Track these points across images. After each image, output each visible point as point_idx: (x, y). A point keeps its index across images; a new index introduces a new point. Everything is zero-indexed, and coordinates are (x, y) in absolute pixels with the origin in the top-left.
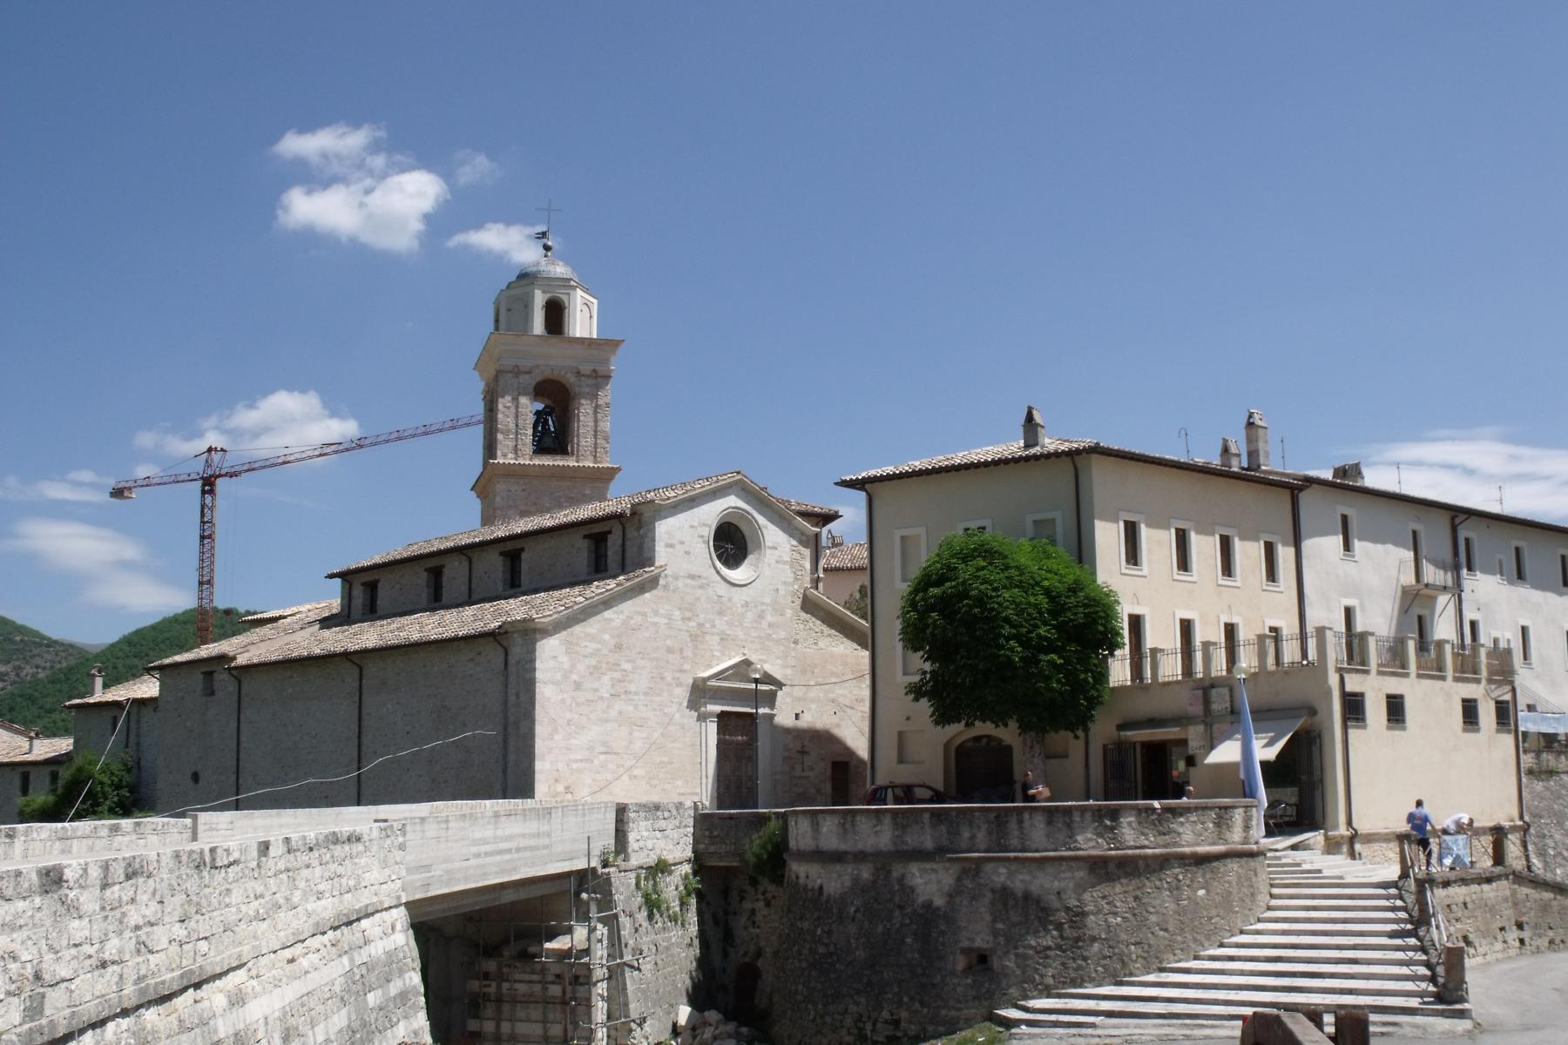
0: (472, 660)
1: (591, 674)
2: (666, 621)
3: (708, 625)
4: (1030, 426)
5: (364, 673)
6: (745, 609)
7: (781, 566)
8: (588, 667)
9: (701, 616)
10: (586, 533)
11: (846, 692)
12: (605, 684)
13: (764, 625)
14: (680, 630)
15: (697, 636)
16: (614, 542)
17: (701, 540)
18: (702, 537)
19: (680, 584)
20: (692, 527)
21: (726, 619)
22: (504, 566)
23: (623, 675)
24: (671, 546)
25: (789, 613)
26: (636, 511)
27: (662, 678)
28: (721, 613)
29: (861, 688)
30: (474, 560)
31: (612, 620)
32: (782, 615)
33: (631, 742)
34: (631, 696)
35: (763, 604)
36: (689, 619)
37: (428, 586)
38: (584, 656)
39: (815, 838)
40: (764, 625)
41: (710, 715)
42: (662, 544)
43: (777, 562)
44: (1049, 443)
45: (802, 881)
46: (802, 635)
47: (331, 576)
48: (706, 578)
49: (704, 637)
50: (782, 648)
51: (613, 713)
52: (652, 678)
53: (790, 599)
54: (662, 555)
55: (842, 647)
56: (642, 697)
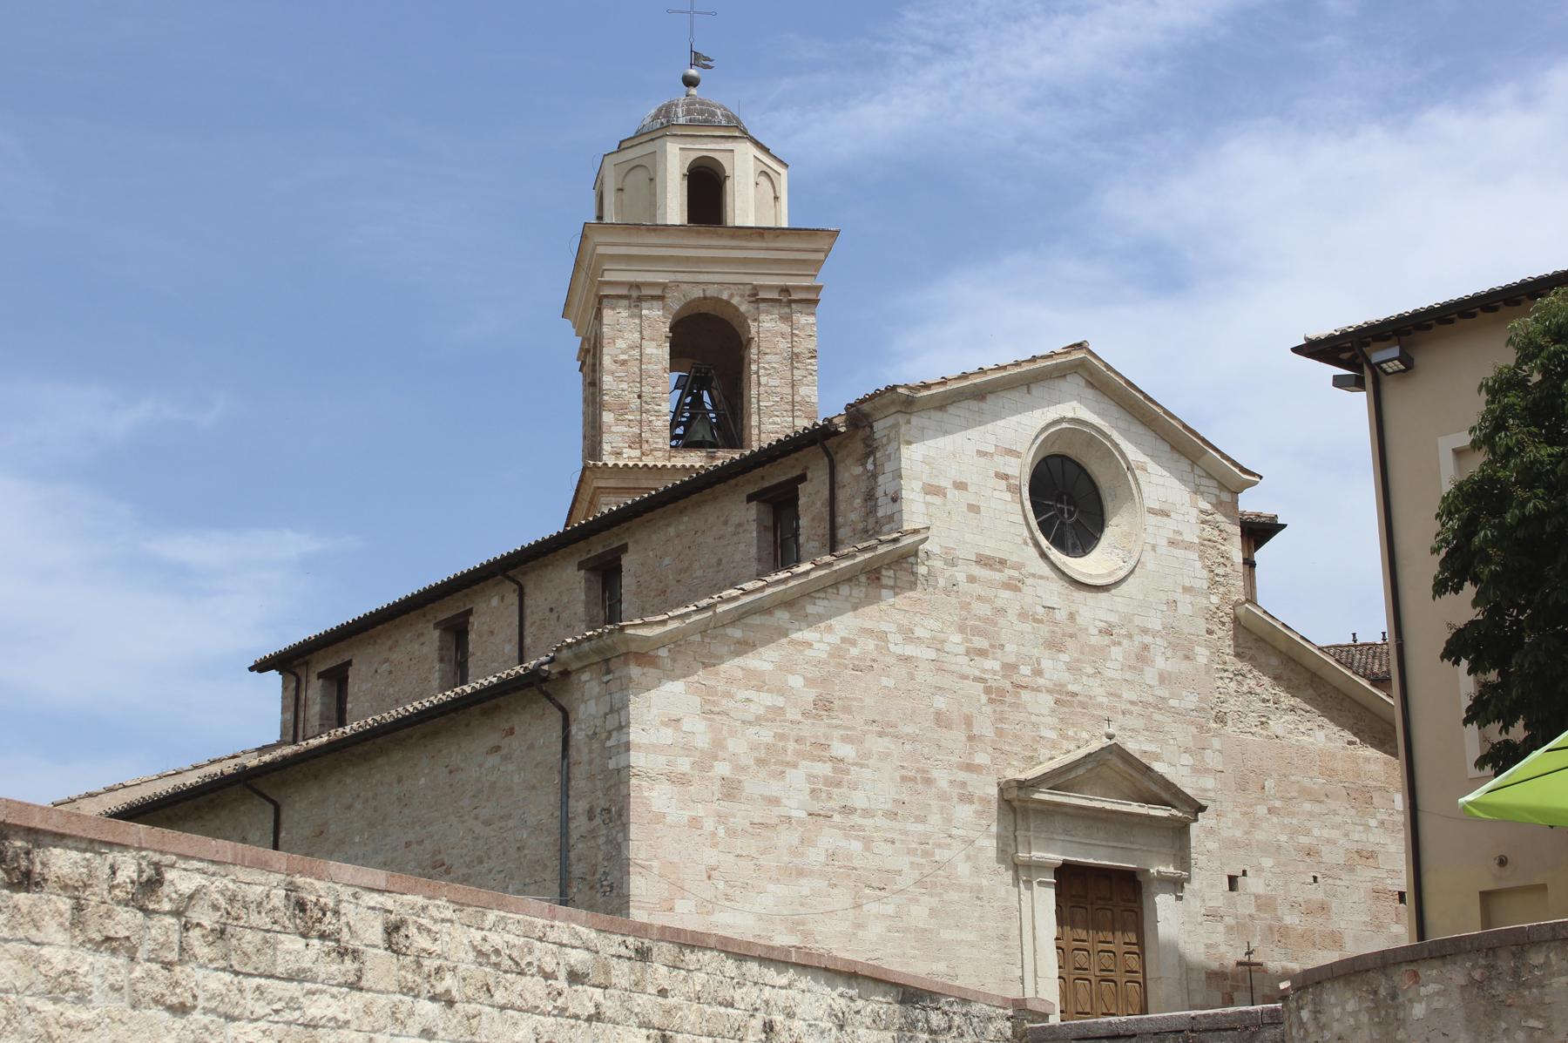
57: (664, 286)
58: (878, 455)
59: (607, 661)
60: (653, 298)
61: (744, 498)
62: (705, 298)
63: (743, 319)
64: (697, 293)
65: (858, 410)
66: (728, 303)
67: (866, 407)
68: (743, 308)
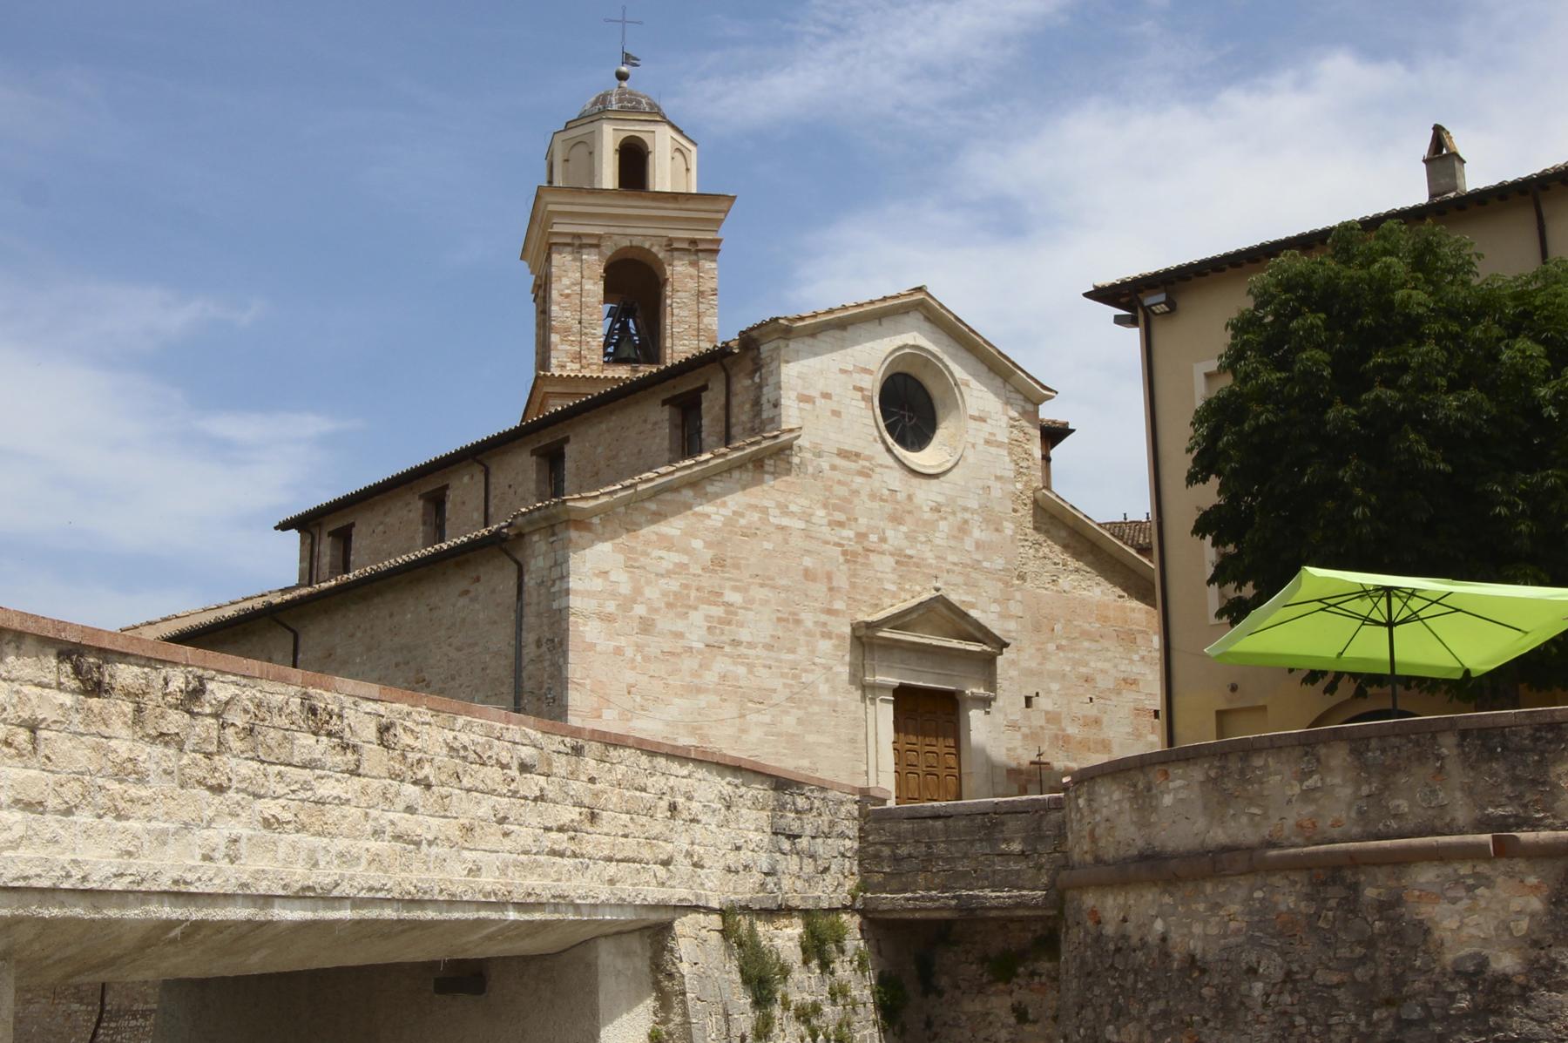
0: (466, 592)
1: (669, 605)
2: (802, 525)
3: (873, 538)
4: (1441, 156)
5: (301, 642)
6: (936, 516)
7: (993, 450)
8: (665, 594)
9: (862, 521)
10: (667, 395)
11: (1107, 666)
12: (695, 627)
13: (969, 544)
14: (827, 543)
15: (855, 554)
16: (711, 403)
17: (859, 394)
18: (861, 389)
19: (825, 464)
20: (843, 371)
21: (904, 529)
22: (539, 471)
23: (727, 612)
24: (805, 398)
25: (1009, 528)
26: (750, 340)
27: (798, 622)
28: (896, 519)
29: (1132, 661)
30: (493, 470)
31: (708, 516)
32: (997, 530)
33: (743, 731)
34: (742, 650)
35: (965, 509)
36: (841, 524)
37: (424, 523)
38: (657, 575)
39: (1143, 824)
40: (969, 544)
41: (882, 688)
42: (793, 395)
43: (987, 442)
44: (1475, 178)
45: (1109, 930)
46: (1032, 567)
47: (284, 526)
48: (869, 458)
49: (867, 557)
50: (1001, 585)
51: (710, 677)
52: (779, 619)
53: (1010, 506)
54: (791, 414)
55: (1097, 591)
56: (760, 651)
57: (599, 237)
58: (763, 371)
59: (552, 526)
60: (592, 246)
61: (659, 402)
62: (631, 247)
63: (660, 263)
64: (625, 243)
65: (749, 336)
66: (649, 251)
67: (755, 334)
68: (661, 256)
